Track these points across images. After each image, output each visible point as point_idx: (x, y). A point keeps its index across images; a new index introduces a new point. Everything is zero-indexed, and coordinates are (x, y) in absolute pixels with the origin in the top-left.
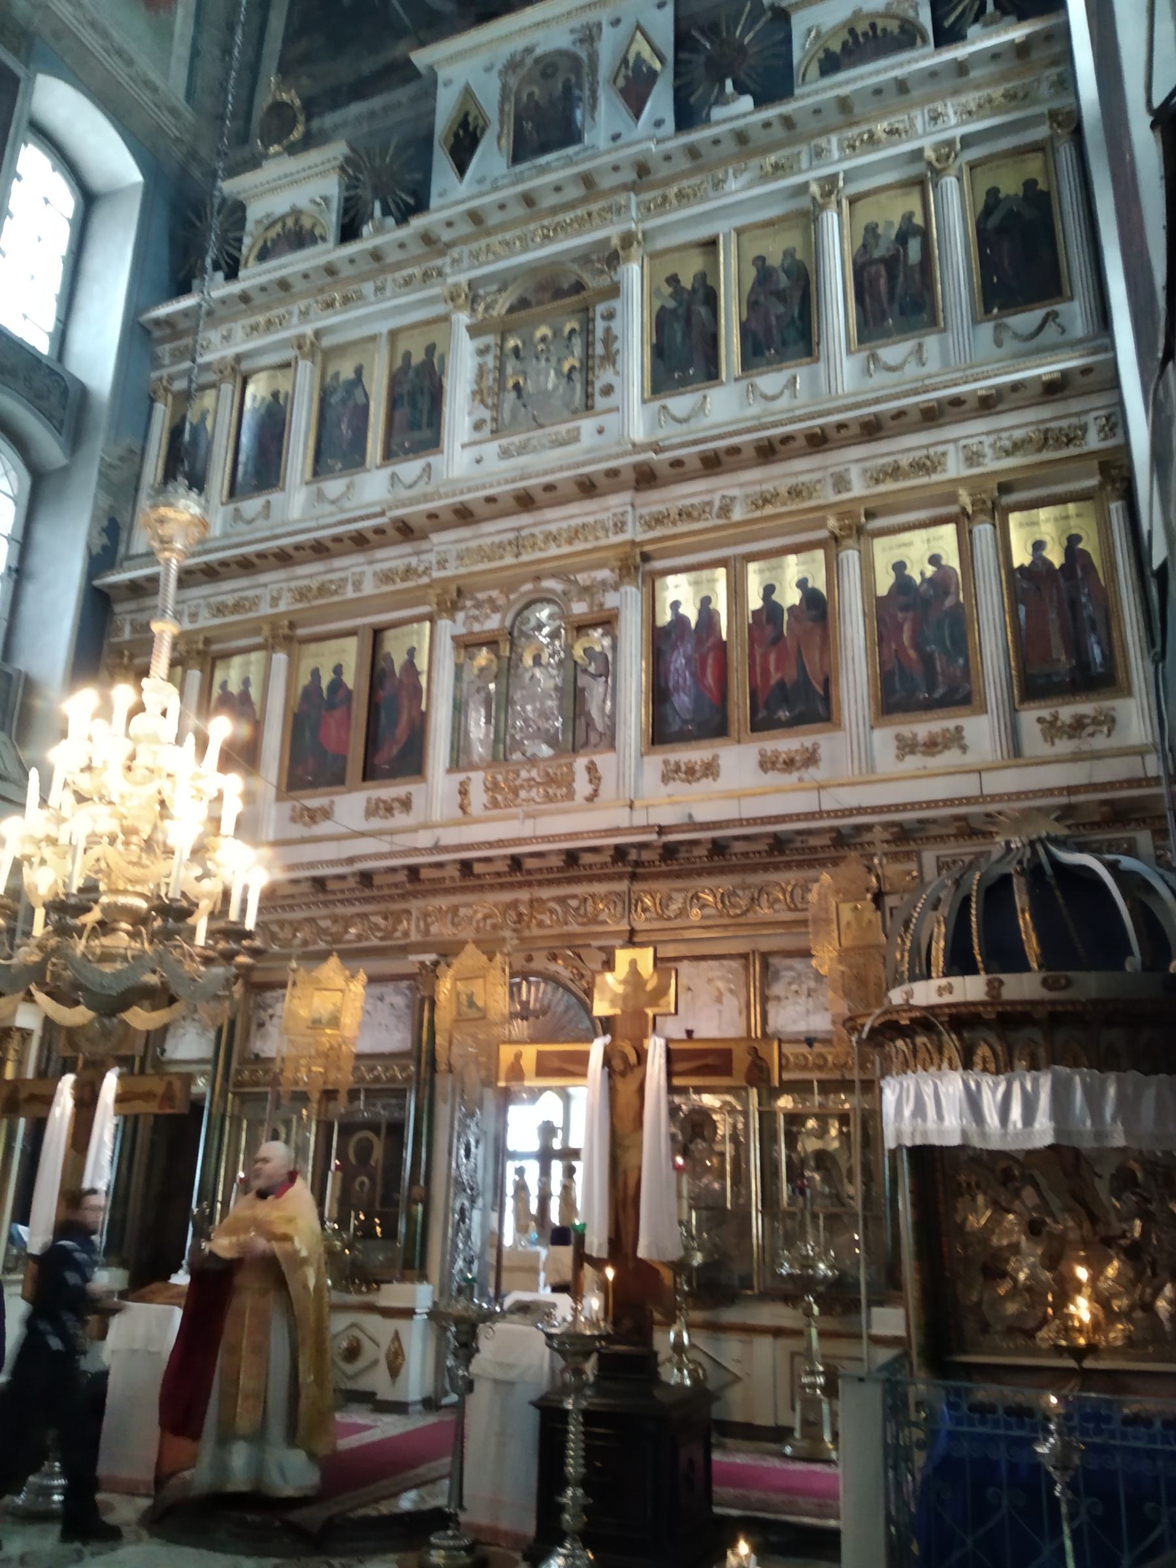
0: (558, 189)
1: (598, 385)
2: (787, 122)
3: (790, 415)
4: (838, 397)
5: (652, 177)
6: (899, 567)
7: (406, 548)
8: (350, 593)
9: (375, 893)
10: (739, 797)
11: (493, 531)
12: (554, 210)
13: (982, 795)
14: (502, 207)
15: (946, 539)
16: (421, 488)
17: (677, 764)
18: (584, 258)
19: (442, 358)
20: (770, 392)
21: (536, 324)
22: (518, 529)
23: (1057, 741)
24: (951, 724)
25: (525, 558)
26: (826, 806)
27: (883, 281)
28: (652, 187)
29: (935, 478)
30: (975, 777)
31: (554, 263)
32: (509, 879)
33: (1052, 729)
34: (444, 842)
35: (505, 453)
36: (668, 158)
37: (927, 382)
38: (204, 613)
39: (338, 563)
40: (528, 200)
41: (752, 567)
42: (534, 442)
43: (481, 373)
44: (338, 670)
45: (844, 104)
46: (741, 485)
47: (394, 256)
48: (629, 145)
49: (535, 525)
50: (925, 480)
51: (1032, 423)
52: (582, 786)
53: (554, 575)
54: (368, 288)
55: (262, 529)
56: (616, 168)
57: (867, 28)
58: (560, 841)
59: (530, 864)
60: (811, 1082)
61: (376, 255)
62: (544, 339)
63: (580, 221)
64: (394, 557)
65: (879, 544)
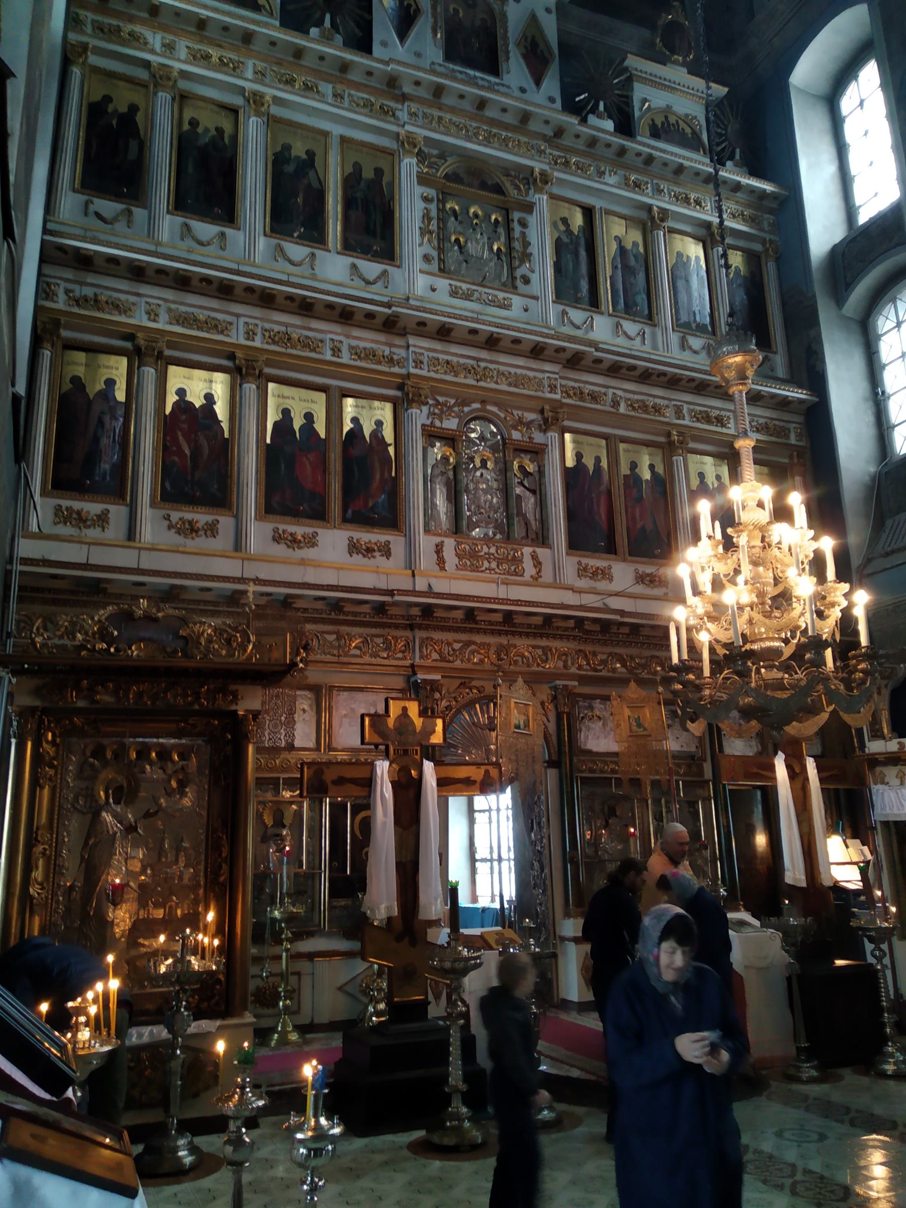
0: (504, 110)
1: (519, 273)
2: (622, 151)
3: (628, 352)
4: (253, 265)
5: (559, 141)
6: (181, 392)
7: (382, 337)
8: (328, 356)
9: (341, 617)
10: (338, 569)
11: (458, 353)
12: (493, 122)
13: (242, 578)
14: (462, 97)
15: (219, 385)
16: (579, 333)
17: (587, 565)
18: (508, 170)
19: (391, 184)
20: (204, 238)
21: (474, 202)
22: (478, 360)
23: (355, 555)
24: (309, 530)
25: (482, 384)
26: (144, 566)
27: (571, 264)
28: (557, 147)
29: (122, 319)
30: (137, 551)
31: (482, 159)
32: (600, 637)
33: (583, 571)
34: (437, 589)
35: (454, 293)
36: (577, 136)
37: (480, 317)
38: (164, 316)
39: (315, 324)
40: (482, 104)
41: (349, 402)
42: (476, 295)
43: (427, 217)
44: (309, 417)
45: (649, 160)
46: (625, 390)
47: (354, 76)
48: (526, 102)
49: (491, 362)
50: (719, 429)
51: (766, 418)
52: (529, 569)
53: (495, 404)
54: (327, 88)
55: (298, 275)
56: (547, 122)
57: (663, 119)
58: (347, 592)
59: (518, 620)
60: (279, 778)
61: (299, 53)
62: (476, 216)
63: (506, 140)
64: (367, 339)
65: (173, 370)
